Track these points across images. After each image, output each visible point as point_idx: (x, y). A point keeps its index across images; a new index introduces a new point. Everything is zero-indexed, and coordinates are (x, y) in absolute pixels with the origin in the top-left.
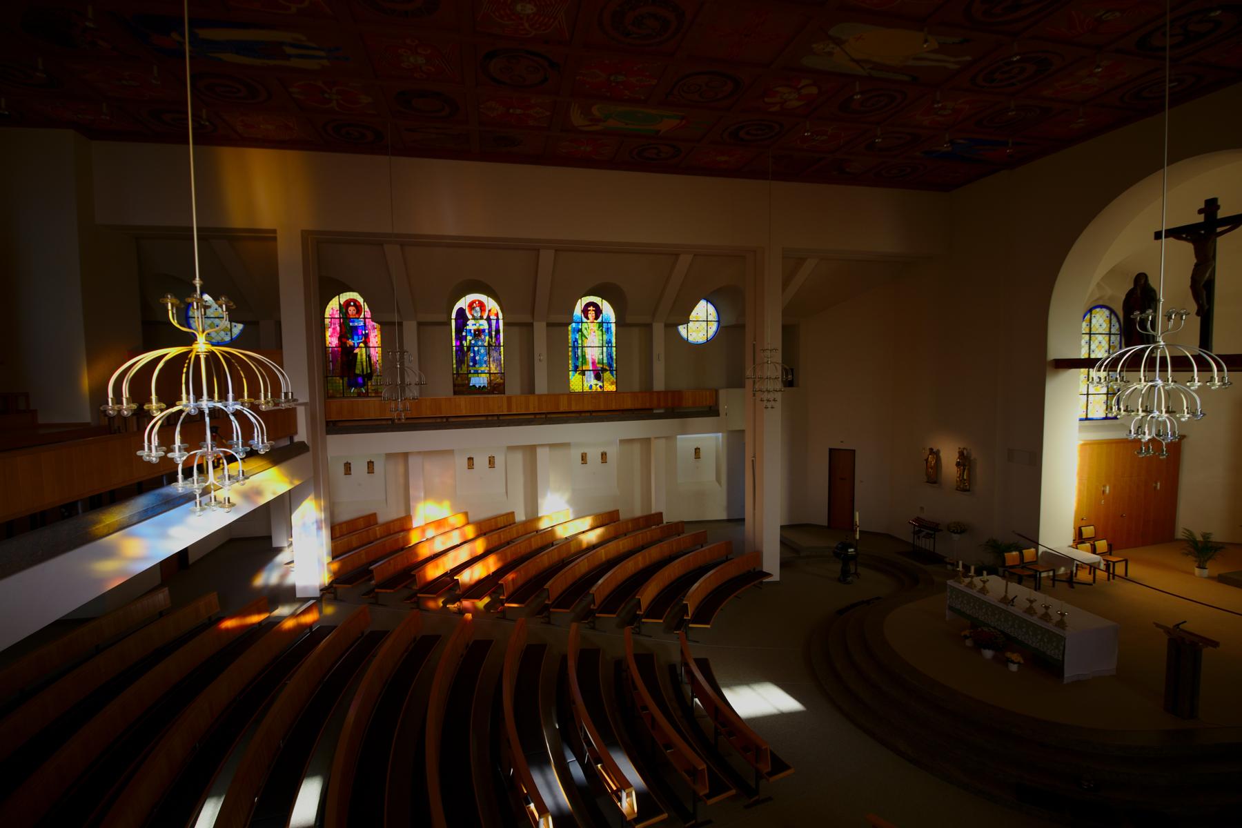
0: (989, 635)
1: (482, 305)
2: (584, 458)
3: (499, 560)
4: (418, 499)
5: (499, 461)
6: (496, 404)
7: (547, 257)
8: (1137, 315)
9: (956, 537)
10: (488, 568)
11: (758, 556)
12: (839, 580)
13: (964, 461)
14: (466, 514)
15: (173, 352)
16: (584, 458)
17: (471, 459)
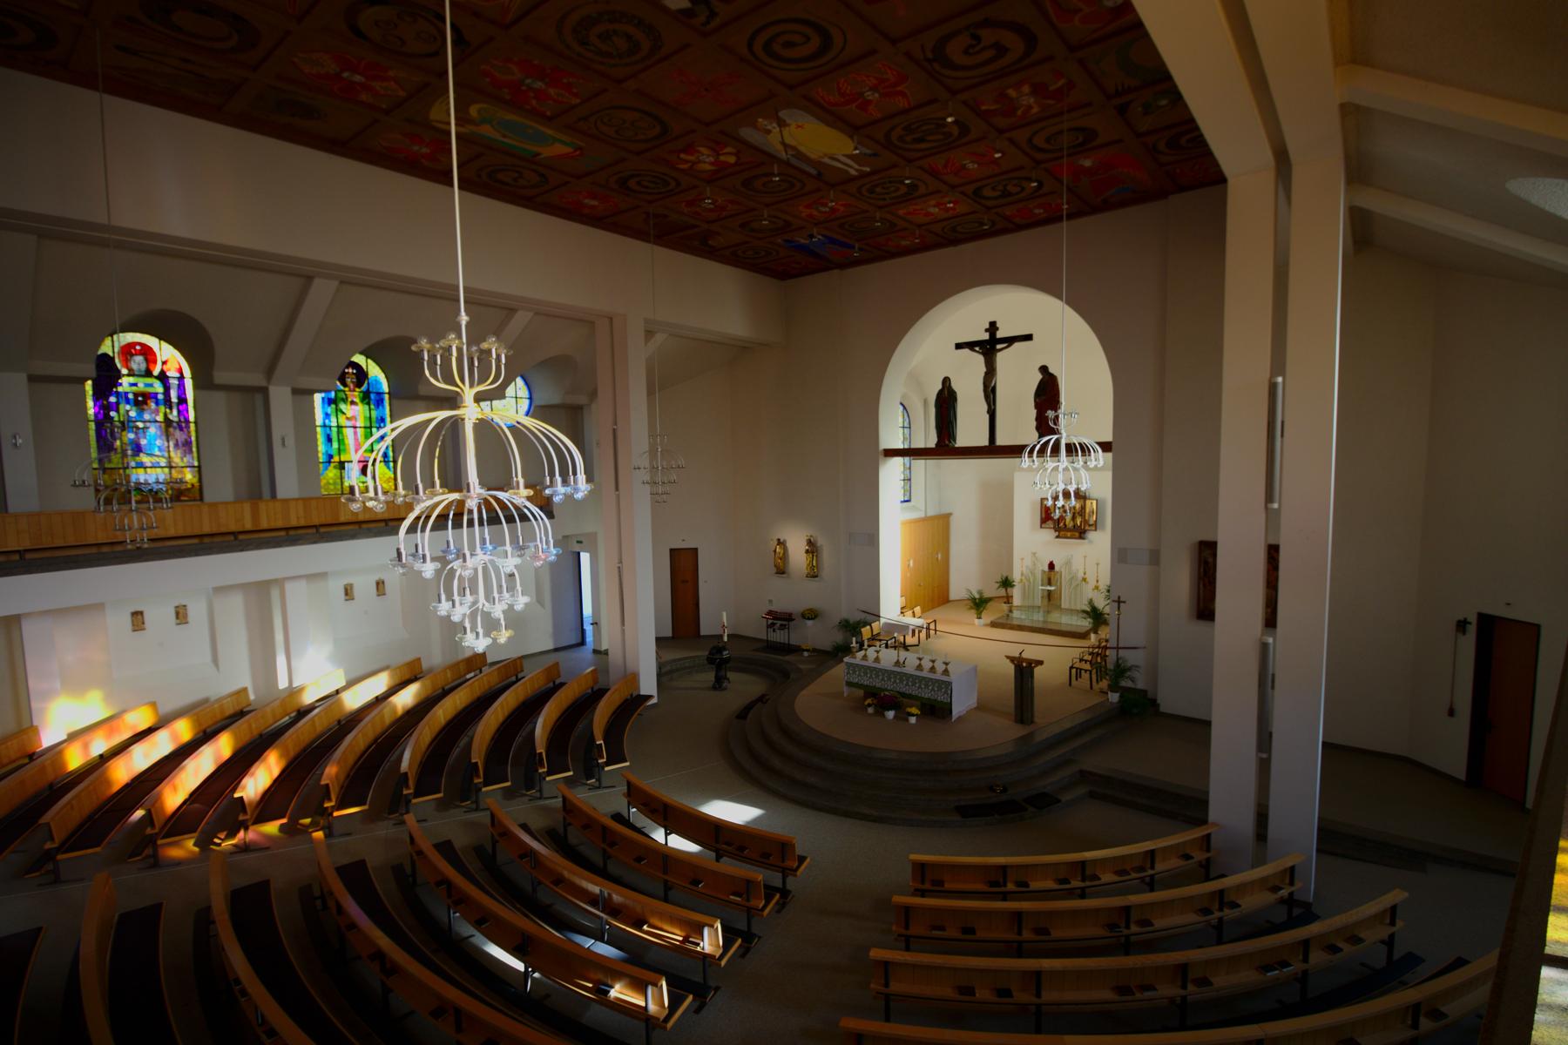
0: (884, 697)
1: (148, 353)
2: (348, 592)
3: (282, 756)
4: (48, 695)
5: (197, 611)
6: (171, 521)
7: (322, 291)
8: (1051, 414)
9: (810, 623)
10: (270, 772)
11: (634, 678)
12: (714, 688)
13: (812, 548)
14: (153, 705)
15: (442, 415)
16: (348, 592)
17: (137, 615)
